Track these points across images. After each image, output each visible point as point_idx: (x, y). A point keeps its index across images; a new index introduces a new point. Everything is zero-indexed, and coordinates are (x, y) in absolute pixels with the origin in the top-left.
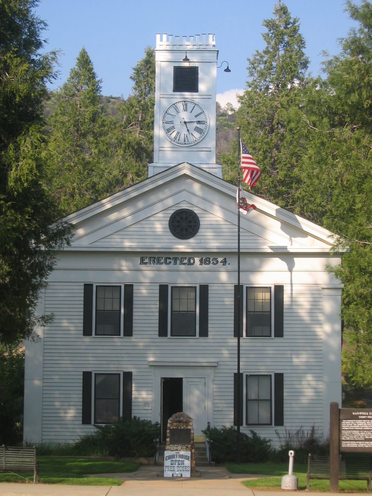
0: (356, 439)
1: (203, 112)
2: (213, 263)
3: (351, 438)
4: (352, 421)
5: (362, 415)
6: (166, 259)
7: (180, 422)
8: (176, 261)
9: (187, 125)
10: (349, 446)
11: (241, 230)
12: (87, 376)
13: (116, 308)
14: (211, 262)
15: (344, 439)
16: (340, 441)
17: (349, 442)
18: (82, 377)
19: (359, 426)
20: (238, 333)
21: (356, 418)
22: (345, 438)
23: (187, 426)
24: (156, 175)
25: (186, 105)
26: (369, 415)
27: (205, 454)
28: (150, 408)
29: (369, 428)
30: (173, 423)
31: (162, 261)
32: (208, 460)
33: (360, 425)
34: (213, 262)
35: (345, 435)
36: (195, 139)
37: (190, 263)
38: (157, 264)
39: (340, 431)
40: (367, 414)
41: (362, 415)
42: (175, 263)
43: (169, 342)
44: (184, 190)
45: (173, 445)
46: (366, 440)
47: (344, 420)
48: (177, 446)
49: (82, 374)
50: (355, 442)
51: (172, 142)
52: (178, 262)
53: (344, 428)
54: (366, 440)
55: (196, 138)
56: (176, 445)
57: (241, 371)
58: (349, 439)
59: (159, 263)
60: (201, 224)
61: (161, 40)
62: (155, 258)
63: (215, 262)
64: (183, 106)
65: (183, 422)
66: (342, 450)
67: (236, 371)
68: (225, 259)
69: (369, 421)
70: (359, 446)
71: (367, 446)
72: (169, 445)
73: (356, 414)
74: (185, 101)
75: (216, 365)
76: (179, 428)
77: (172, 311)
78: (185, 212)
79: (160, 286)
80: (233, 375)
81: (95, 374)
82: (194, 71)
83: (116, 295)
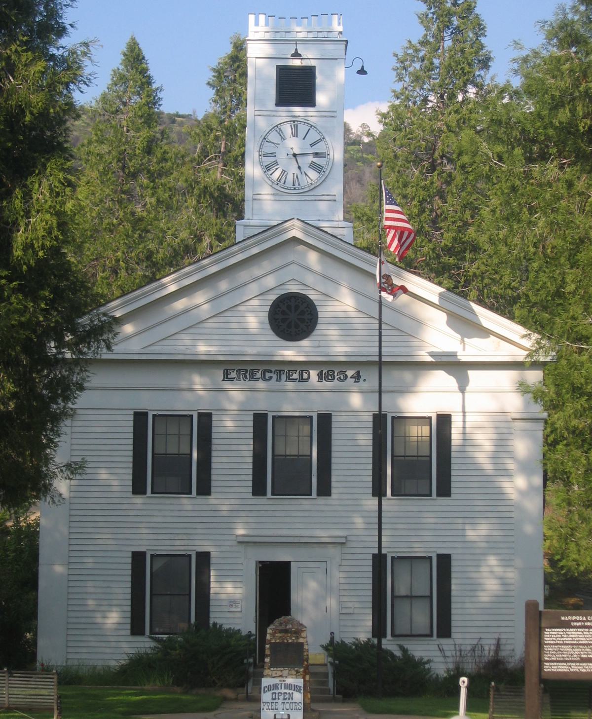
0: (567, 659)
1: (323, 138)
2: (340, 379)
3: (559, 657)
4: (560, 630)
5: (576, 621)
6: (264, 372)
7: (286, 631)
8: (280, 375)
9: (299, 159)
10: (555, 670)
11: (383, 326)
12: (138, 558)
13: (185, 450)
14: (336, 377)
15: (547, 659)
16: (541, 662)
17: (555, 664)
18: (130, 560)
19: (571, 639)
20: (378, 491)
21: (567, 625)
22: (549, 657)
23: (297, 638)
24: (249, 238)
25: (296, 127)
26: (588, 621)
27: (325, 683)
28: (239, 610)
29: (587, 642)
30: (275, 633)
31: (259, 375)
32: (332, 692)
33: (573, 636)
34: (340, 378)
35: (549, 653)
36: (310, 181)
37: (302, 379)
38: (249, 380)
39: (541, 645)
40: (584, 619)
41: (576, 621)
42: (279, 379)
43: (270, 504)
44: (293, 263)
45: (275, 669)
46: (583, 660)
47: (548, 628)
48: (281, 671)
49: (130, 555)
50: (565, 664)
51: (274, 186)
52: (284, 377)
53: (548, 642)
54: (583, 660)
55: (312, 180)
56: (279, 669)
57: (384, 551)
58: (555, 659)
59: (253, 378)
60: (319, 316)
61: (257, 23)
62: (247, 371)
63: (342, 378)
64: (292, 129)
65: (291, 632)
66: (544, 676)
67: (376, 551)
68: (358, 372)
69: (587, 630)
70: (571, 670)
71: (584, 670)
72: (269, 669)
73: (567, 619)
74: (294, 122)
75: (343, 540)
76: (286, 641)
77: (273, 455)
78: (295, 297)
79: (255, 415)
80: (371, 557)
81: (152, 556)
82: (308, 74)
83: (185, 430)
